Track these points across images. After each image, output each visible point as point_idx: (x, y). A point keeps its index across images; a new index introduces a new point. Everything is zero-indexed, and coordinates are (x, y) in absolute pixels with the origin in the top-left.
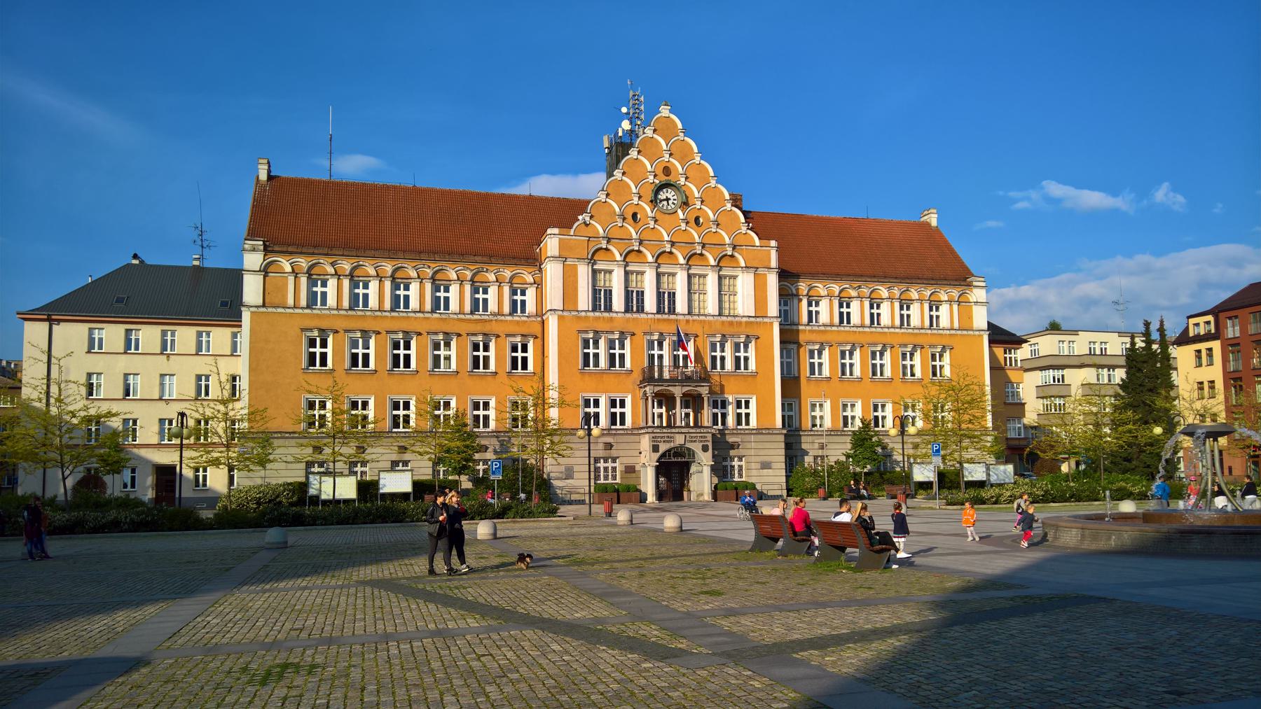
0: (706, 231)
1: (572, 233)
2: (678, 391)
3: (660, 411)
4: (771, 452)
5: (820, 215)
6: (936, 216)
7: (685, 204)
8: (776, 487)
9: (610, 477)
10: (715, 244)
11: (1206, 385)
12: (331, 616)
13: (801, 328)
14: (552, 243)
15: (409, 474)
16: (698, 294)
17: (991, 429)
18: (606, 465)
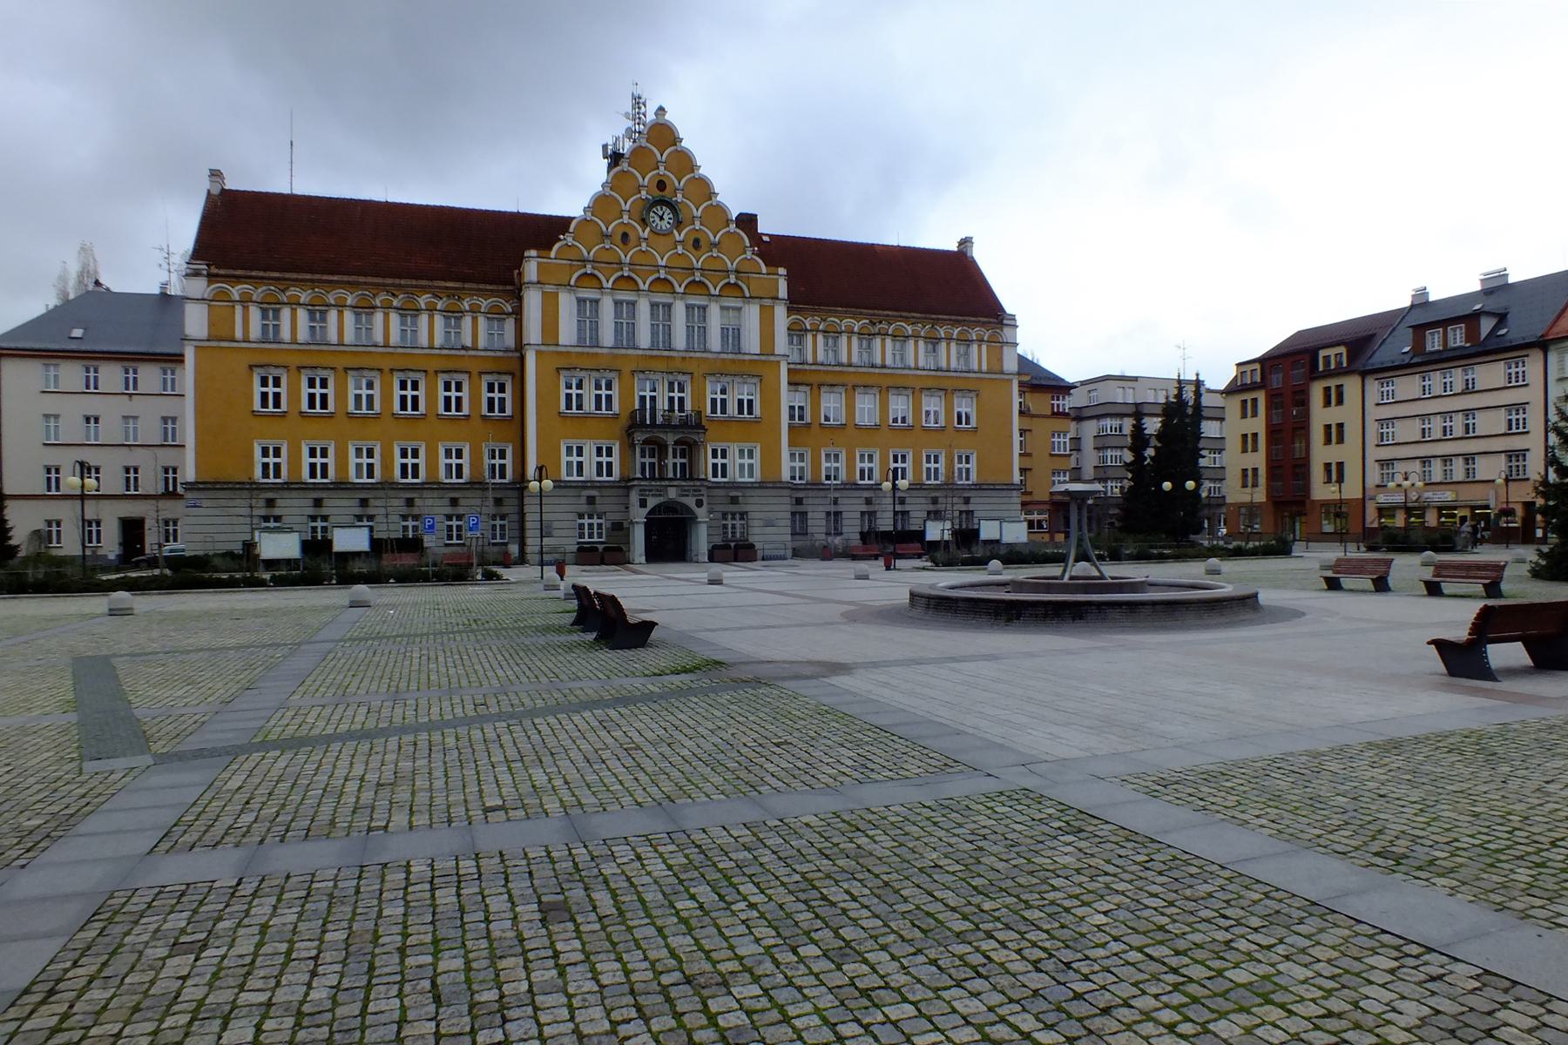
2: (670, 439)
3: (652, 460)
4: (776, 508)
9: (595, 534)
10: (715, 271)
11: (1250, 473)
14: (531, 270)
15: (366, 531)
18: (591, 521)
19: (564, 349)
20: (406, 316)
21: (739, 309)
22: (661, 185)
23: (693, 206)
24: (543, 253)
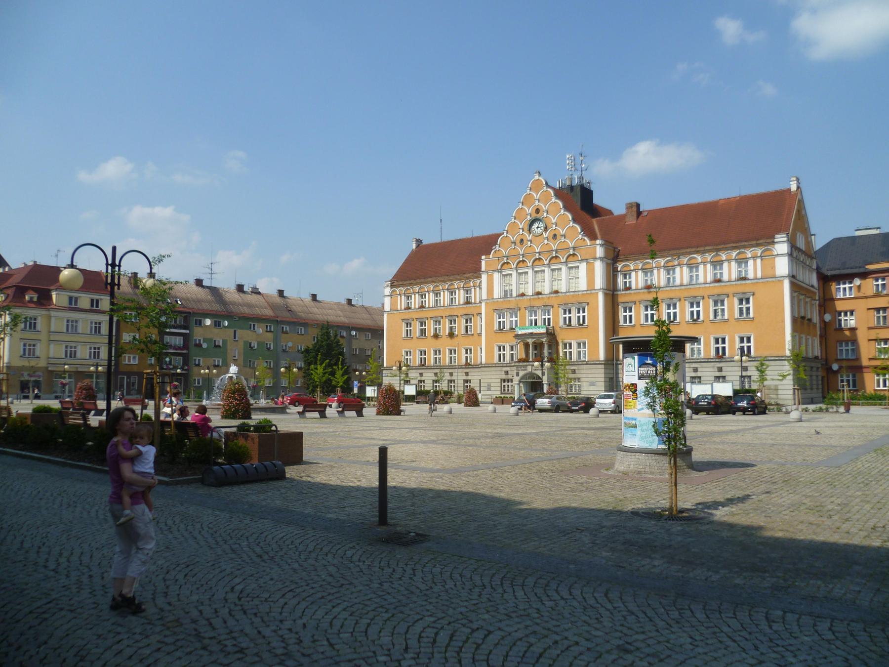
4: (596, 375)
13: (619, 293)
19: (496, 300)
20: (693, 267)
21: (578, 267)
22: (538, 211)
23: (552, 218)
24: (487, 256)
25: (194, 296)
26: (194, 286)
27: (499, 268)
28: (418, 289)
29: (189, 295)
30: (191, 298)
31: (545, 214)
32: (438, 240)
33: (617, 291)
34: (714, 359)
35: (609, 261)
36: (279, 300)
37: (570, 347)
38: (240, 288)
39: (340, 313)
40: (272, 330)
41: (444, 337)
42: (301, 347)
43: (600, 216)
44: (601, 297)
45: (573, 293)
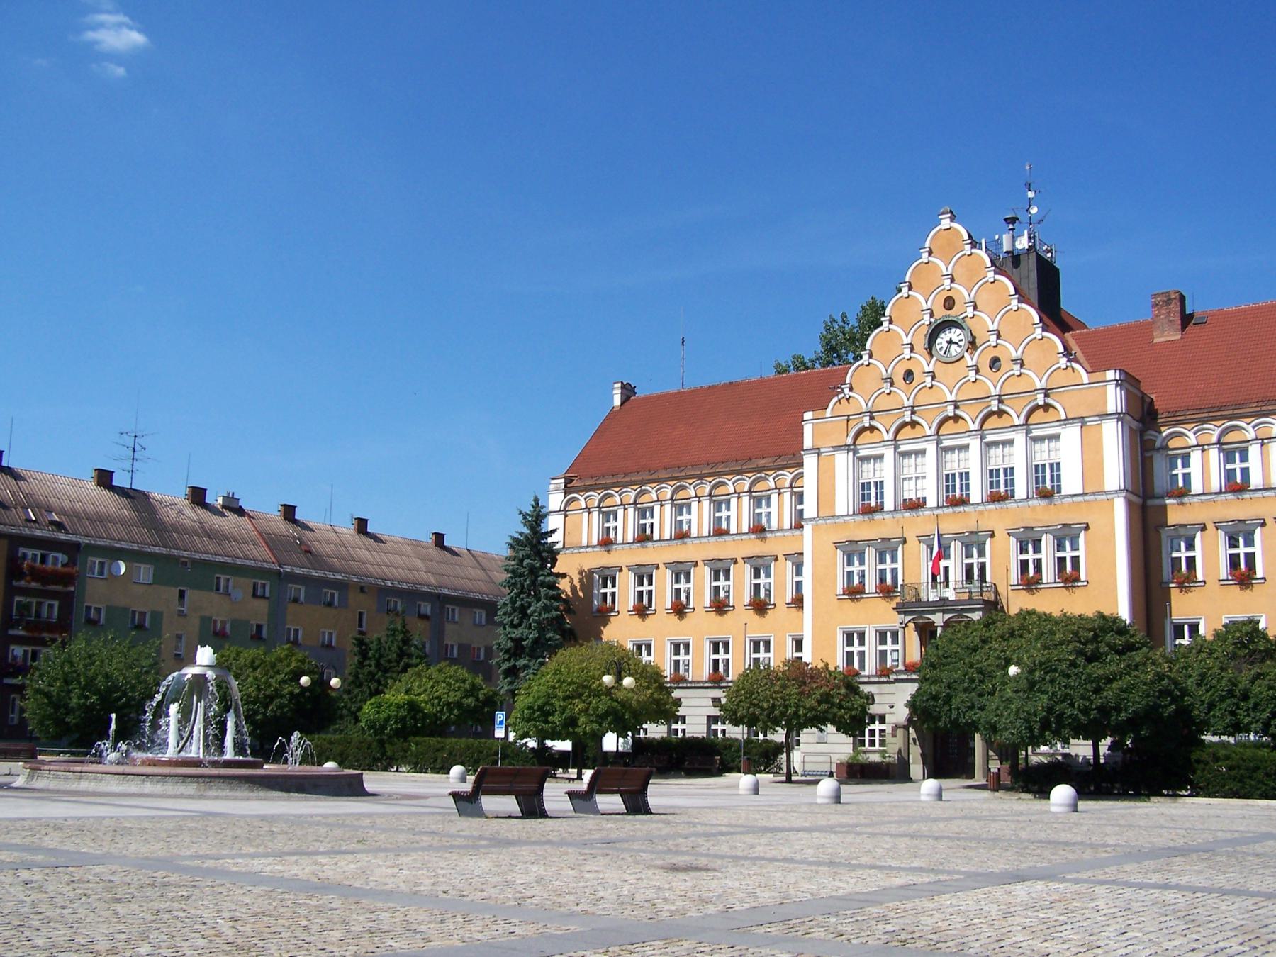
0: (876, 395)
1: (828, 415)
5: (659, 392)
6: (620, 391)
7: (973, 344)
8: (821, 759)
12: (521, 878)
16: (914, 479)
17: (668, 679)
22: (949, 303)
25: (90, 508)
26: (92, 485)
27: (849, 441)
28: (633, 495)
29: (78, 506)
30: (84, 511)
31: (970, 310)
32: (675, 388)
33: (1153, 497)
34: (706, 682)
35: (1135, 424)
36: (284, 528)
37: (862, 643)
38: (198, 496)
39: (419, 564)
40: (267, 594)
41: (781, 607)
42: (330, 634)
43: (1073, 330)
44: (1120, 506)
45: (1069, 500)
